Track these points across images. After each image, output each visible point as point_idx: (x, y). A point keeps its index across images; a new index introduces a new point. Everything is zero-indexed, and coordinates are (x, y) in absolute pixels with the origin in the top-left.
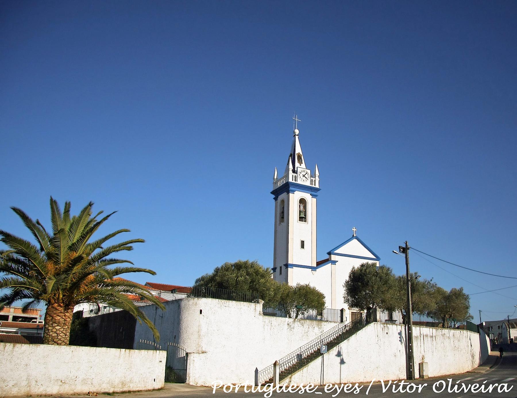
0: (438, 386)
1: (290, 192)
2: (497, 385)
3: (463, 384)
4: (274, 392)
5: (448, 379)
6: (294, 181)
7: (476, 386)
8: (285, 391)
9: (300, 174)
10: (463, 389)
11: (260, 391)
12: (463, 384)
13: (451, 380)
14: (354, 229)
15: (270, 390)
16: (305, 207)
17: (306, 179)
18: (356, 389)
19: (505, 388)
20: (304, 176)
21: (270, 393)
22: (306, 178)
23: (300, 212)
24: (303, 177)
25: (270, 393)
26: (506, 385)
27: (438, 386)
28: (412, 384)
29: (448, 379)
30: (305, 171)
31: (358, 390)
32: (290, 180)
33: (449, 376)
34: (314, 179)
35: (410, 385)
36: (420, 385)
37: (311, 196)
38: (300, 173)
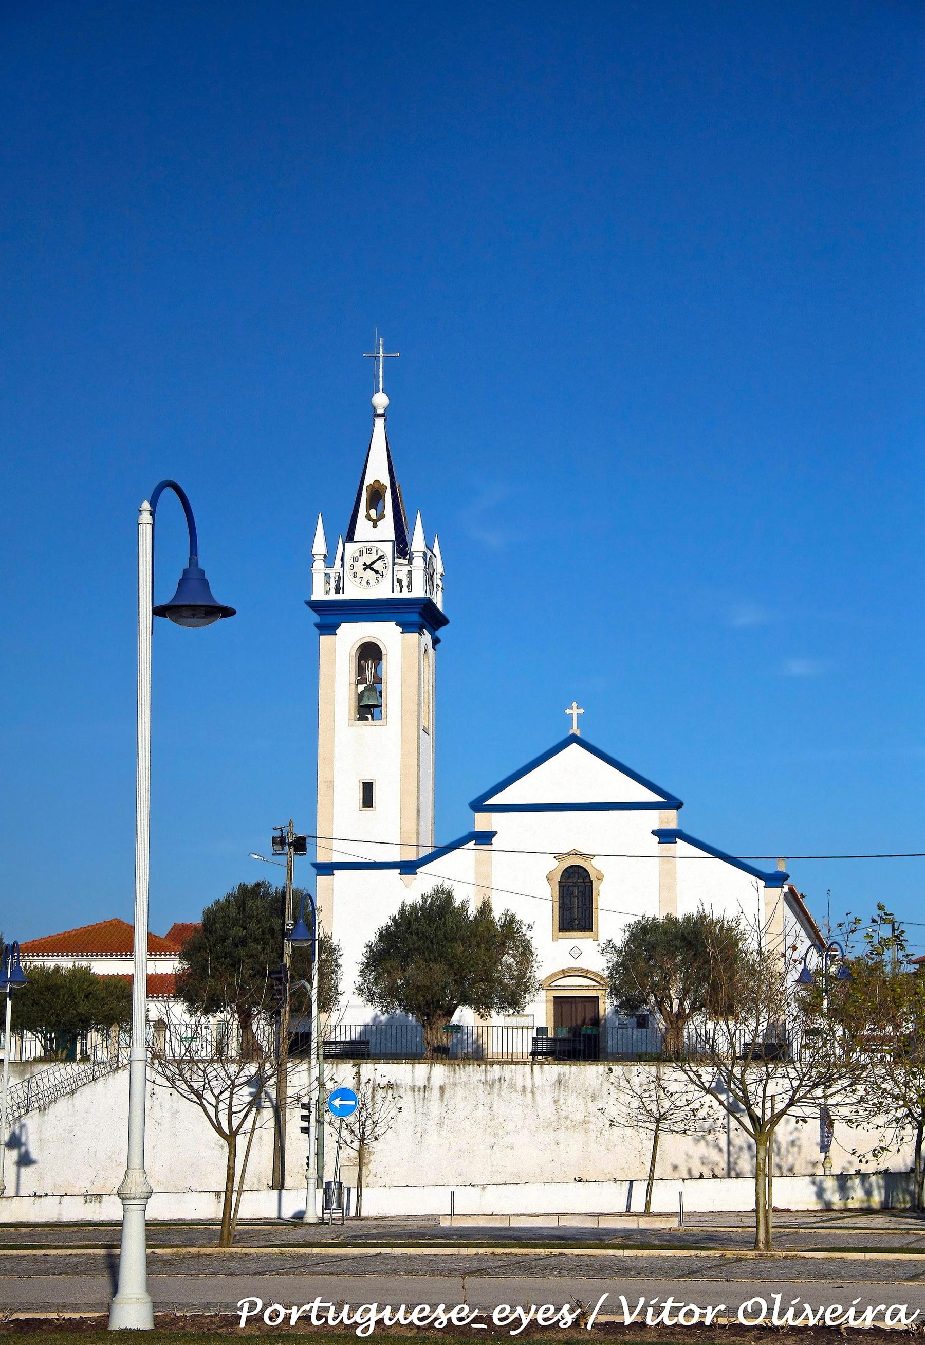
0: (749, 1310)
2: (883, 1307)
3: (807, 1306)
4: (380, 1322)
5: (773, 1295)
6: (333, 596)
8: (403, 1322)
11: (347, 1322)
12: (807, 1306)
13: (778, 1297)
14: (579, 711)
15: (369, 1320)
17: (378, 575)
19: (902, 1315)
21: (369, 1325)
22: (377, 572)
24: (365, 569)
25: (369, 1325)
27: (749, 1310)
28: (690, 1305)
29: (773, 1295)
30: (374, 551)
33: (323, 1211)
38: (355, 559)
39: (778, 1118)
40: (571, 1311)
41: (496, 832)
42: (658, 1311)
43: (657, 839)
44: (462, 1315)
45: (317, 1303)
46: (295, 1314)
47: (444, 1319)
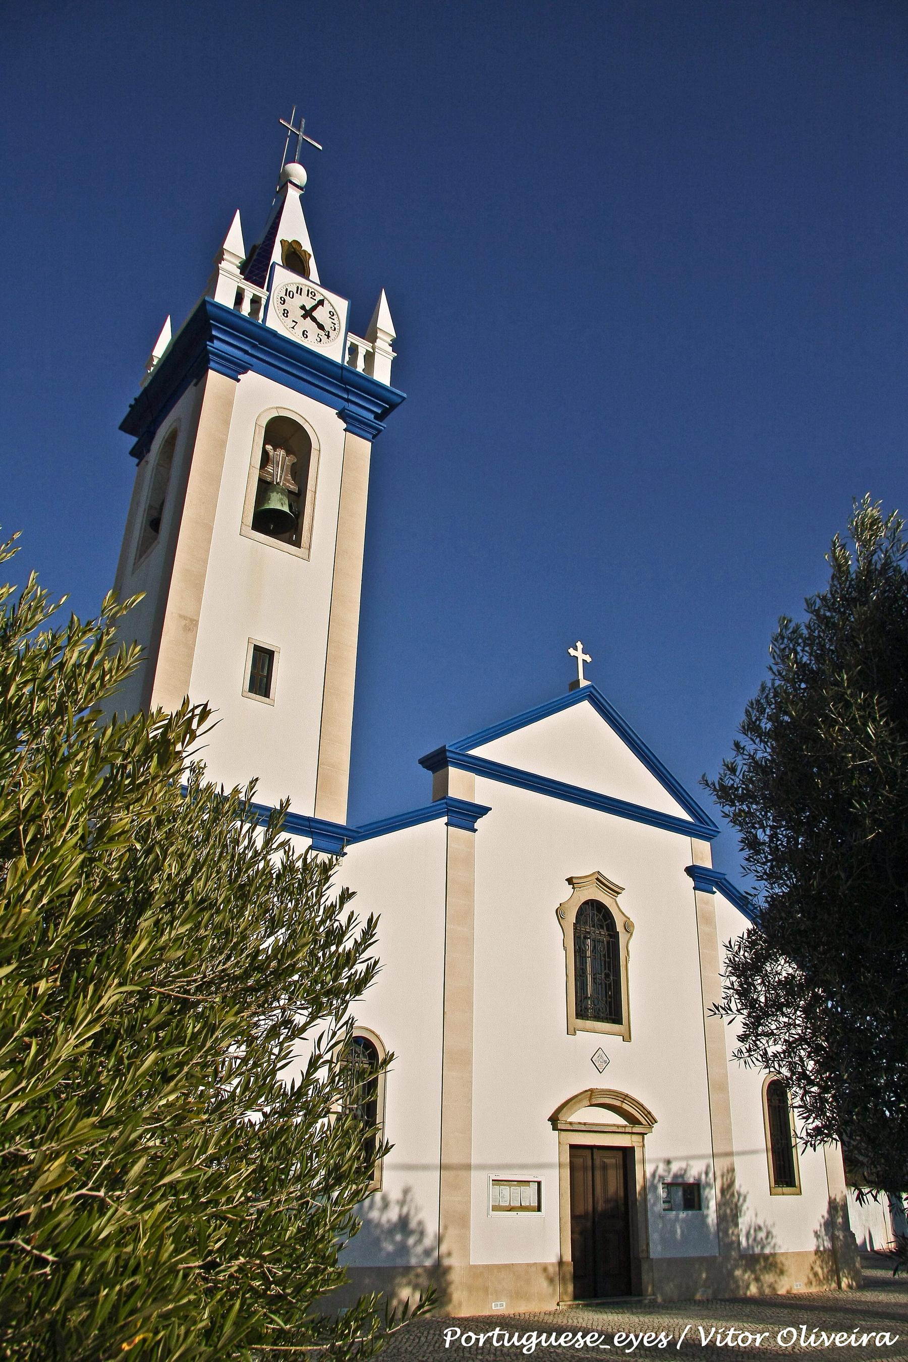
0: (785, 1336)
1: (212, 364)
2: (874, 1334)
5: (801, 1326)
7: (567, 1336)
9: (287, 298)
10: (823, 1341)
16: (300, 472)
18: (661, 1341)
19: (887, 1339)
20: (308, 314)
22: (321, 327)
23: (265, 487)
26: (888, 1335)
29: (801, 1326)
31: (665, 1342)
32: (224, 296)
34: (363, 347)
35: (743, 1335)
36: (482, 1335)
37: (345, 426)
39: (74, 932)
40: (667, 1336)
41: (490, 809)
42: (724, 1336)
43: (690, 882)
44: (842, 1339)
45: (497, 1331)
46: (482, 1338)
47: (582, 1342)
